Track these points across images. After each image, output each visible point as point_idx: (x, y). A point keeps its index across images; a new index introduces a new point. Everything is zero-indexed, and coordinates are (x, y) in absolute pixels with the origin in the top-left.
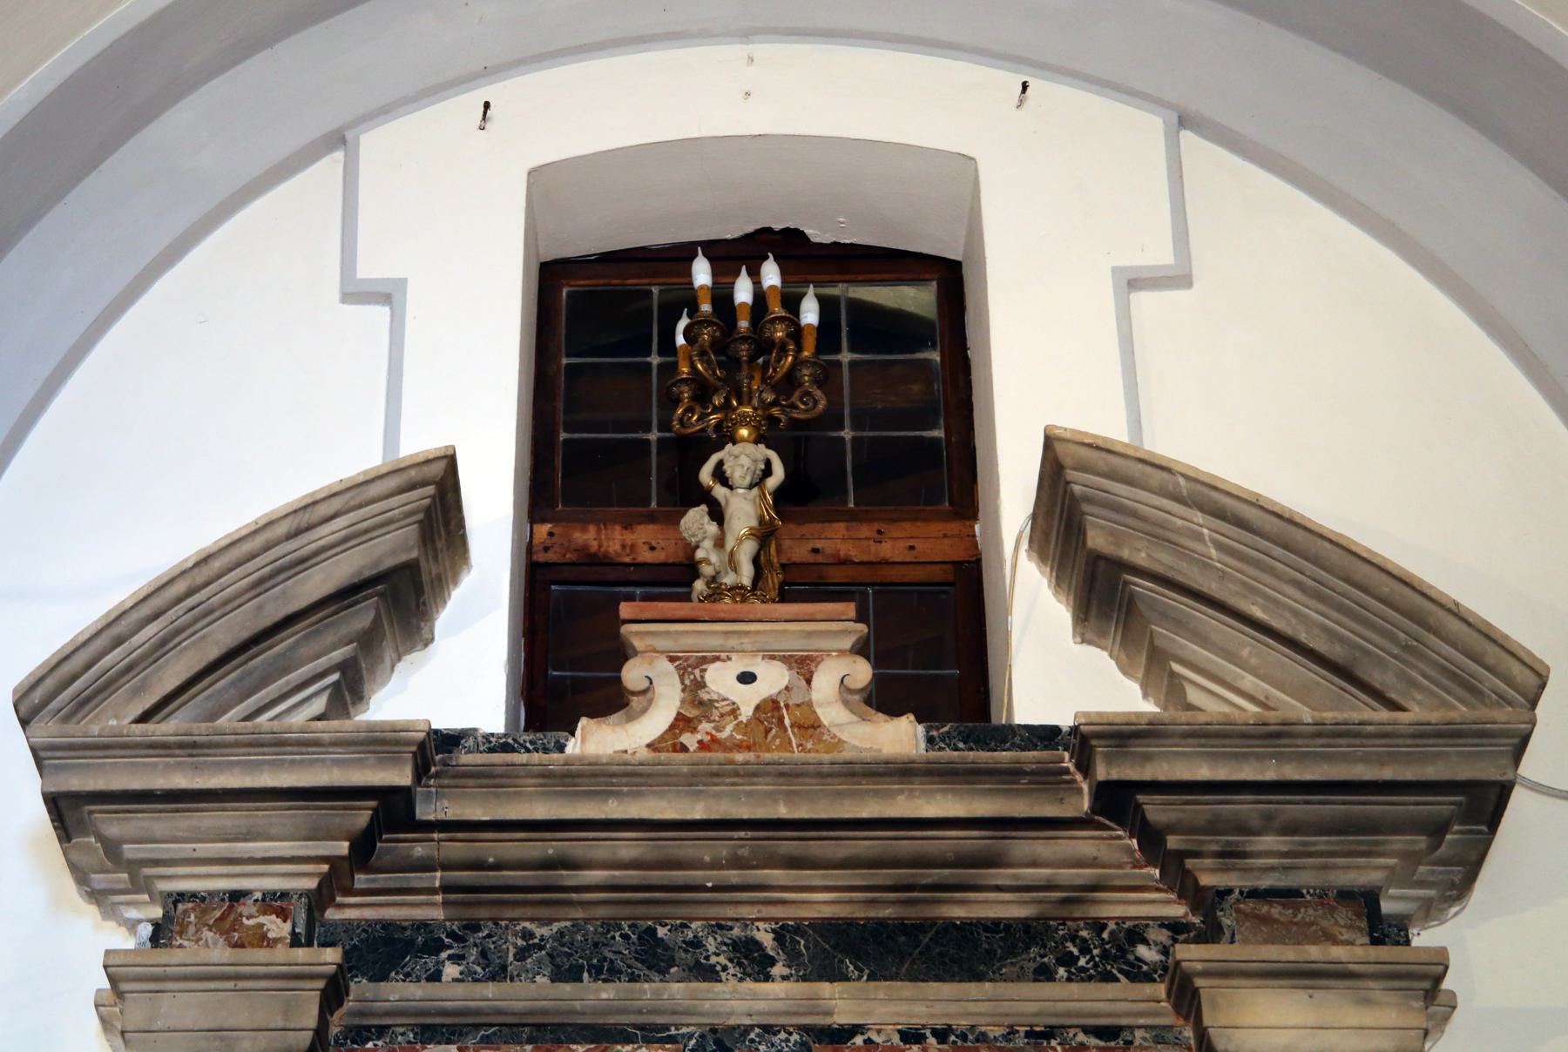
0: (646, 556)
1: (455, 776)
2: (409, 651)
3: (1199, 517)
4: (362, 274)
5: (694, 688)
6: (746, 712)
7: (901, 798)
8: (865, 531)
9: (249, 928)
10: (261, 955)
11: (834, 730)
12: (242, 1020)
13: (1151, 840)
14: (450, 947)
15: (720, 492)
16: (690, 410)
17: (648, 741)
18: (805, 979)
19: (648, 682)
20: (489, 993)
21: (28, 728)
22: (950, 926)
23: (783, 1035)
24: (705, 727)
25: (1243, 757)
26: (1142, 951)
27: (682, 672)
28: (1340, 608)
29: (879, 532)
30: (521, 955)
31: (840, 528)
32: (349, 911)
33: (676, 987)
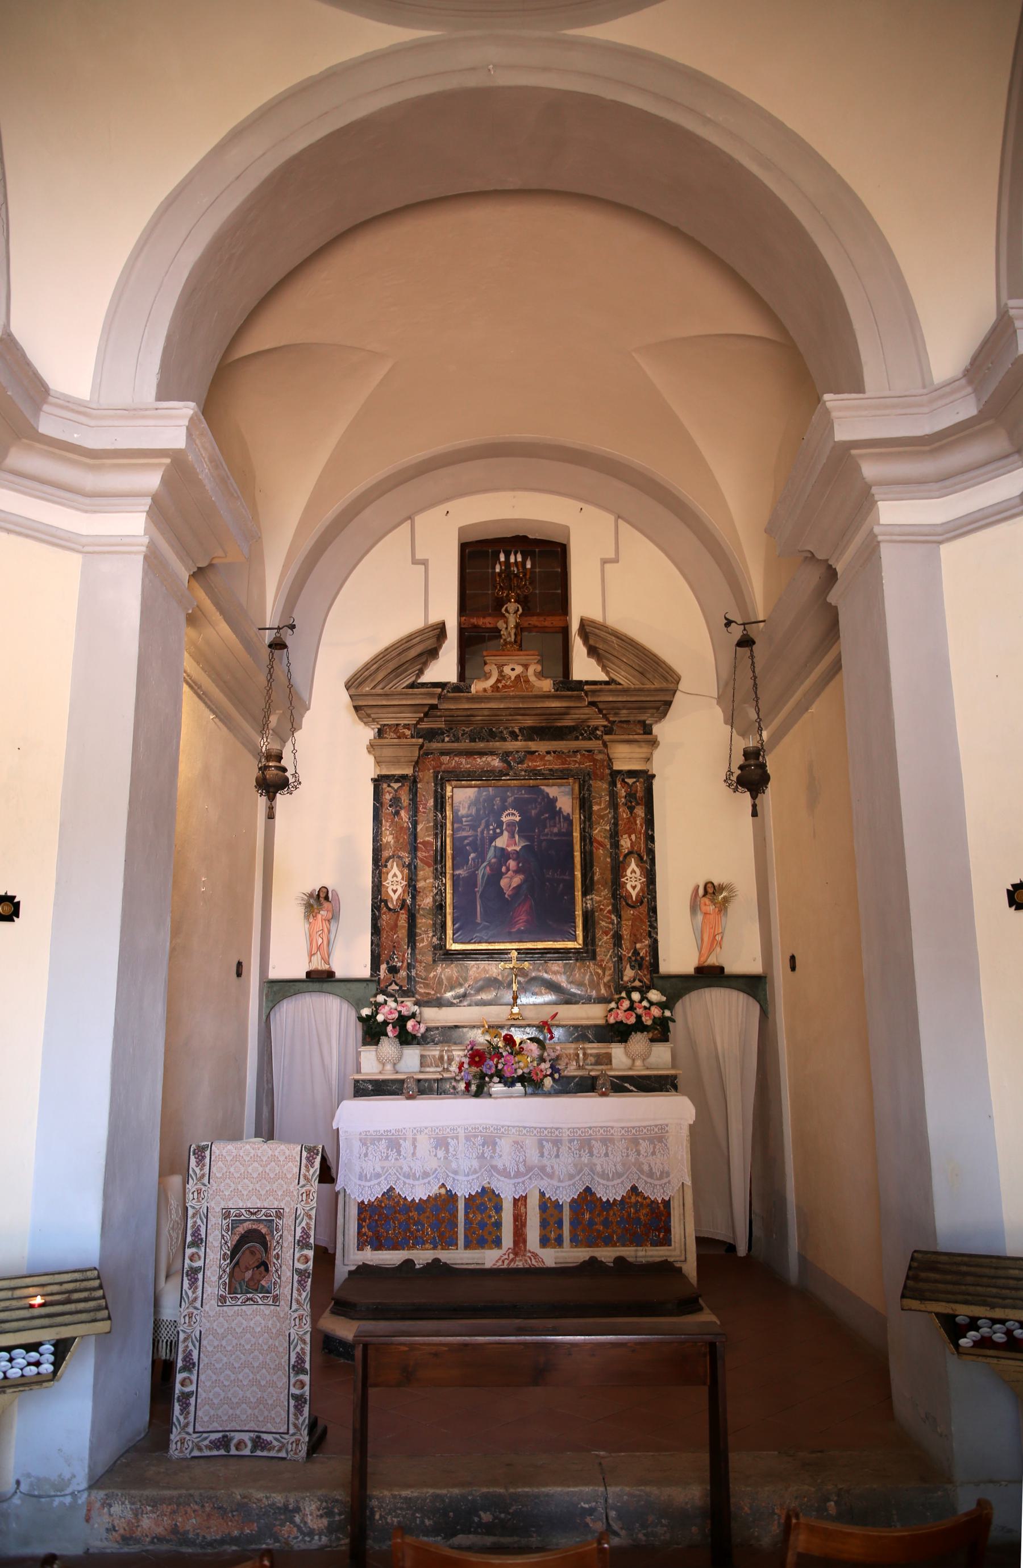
0: (488, 626)
3: (613, 638)
5: (501, 672)
6: (513, 678)
8: (542, 618)
10: (405, 740)
12: (401, 754)
13: (600, 711)
15: (507, 614)
16: (499, 590)
18: (525, 740)
20: (455, 745)
21: (349, 690)
22: (557, 727)
24: (504, 682)
25: (618, 695)
26: (598, 732)
27: (498, 668)
28: (642, 660)
30: (463, 735)
31: (535, 618)
32: (423, 726)
33: (498, 743)
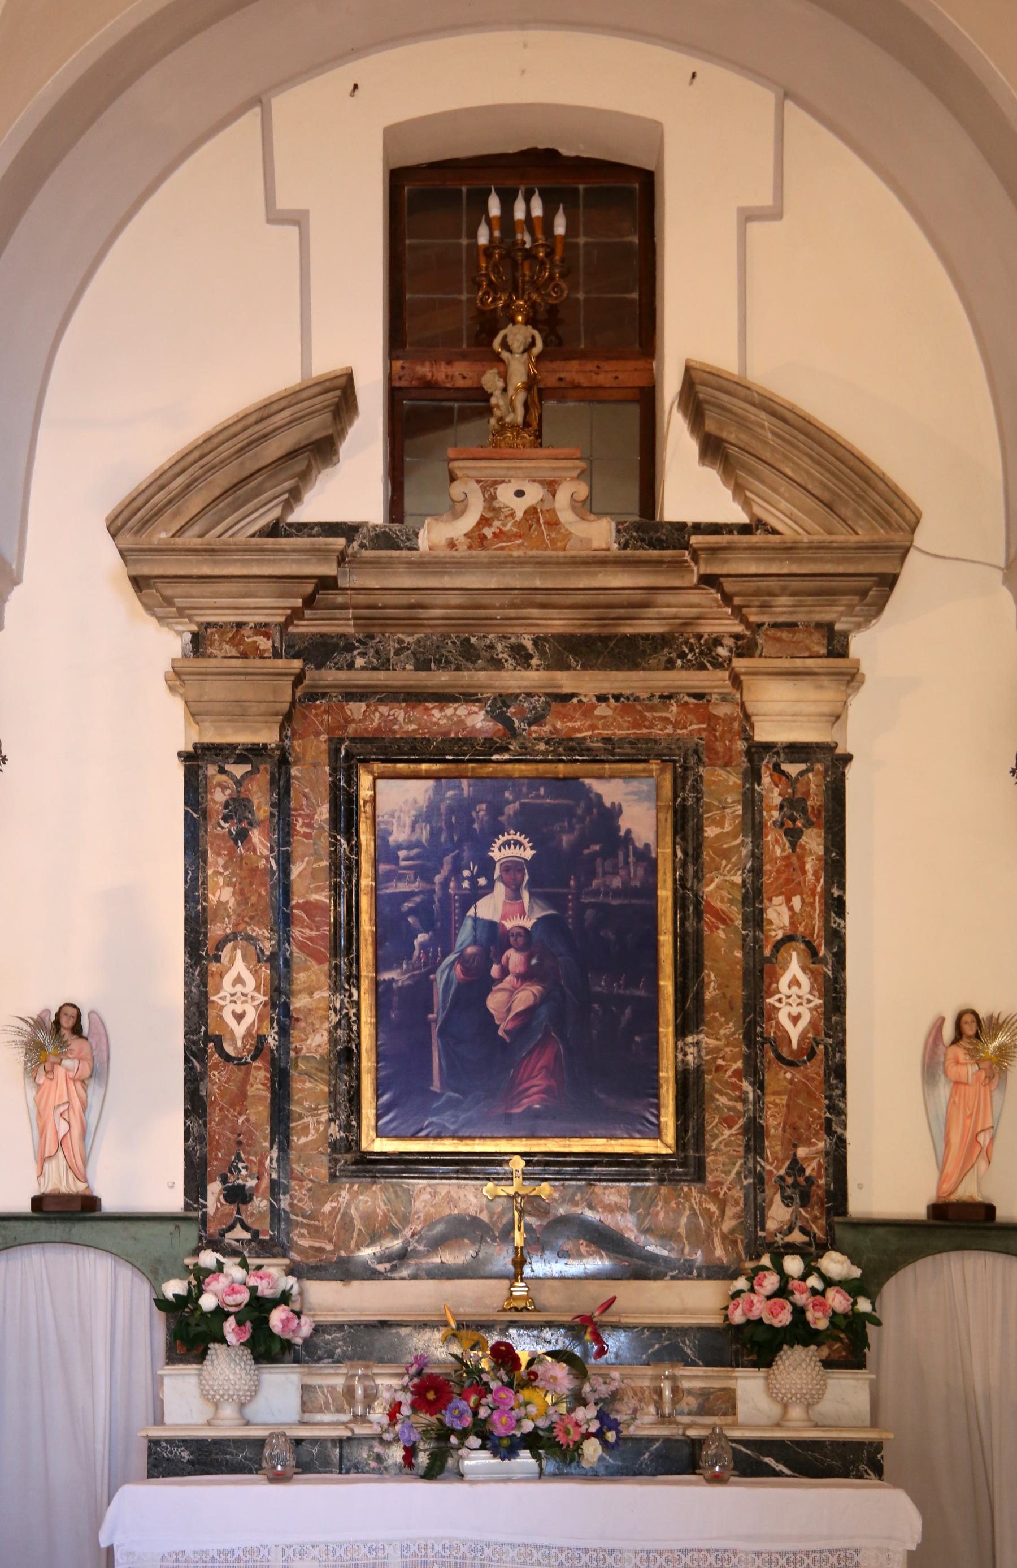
0: (460, 383)
1: (359, 563)
2: (324, 468)
3: (763, 415)
4: (280, 206)
6: (519, 515)
7: (600, 576)
8: (590, 366)
9: (249, 643)
11: (567, 526)
13: (727, 599)
14: (358, 648)
15: (505, 355)
17: (465, 532)
18: (548, 668)
19: (464, 496)
20: (381, 677)
22: (625, 637)
23: (536, 698)
24: (497, 523)
25: (771, 560)
27: (484, 489)
29: (598, 367)
30: (398, 652)
31: (574, 365)
32: (301, 628)
33: (482, 673)
